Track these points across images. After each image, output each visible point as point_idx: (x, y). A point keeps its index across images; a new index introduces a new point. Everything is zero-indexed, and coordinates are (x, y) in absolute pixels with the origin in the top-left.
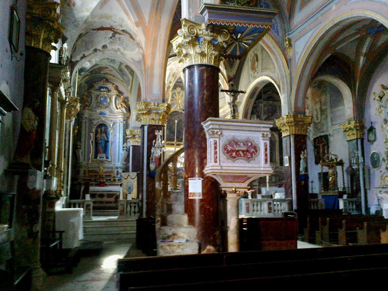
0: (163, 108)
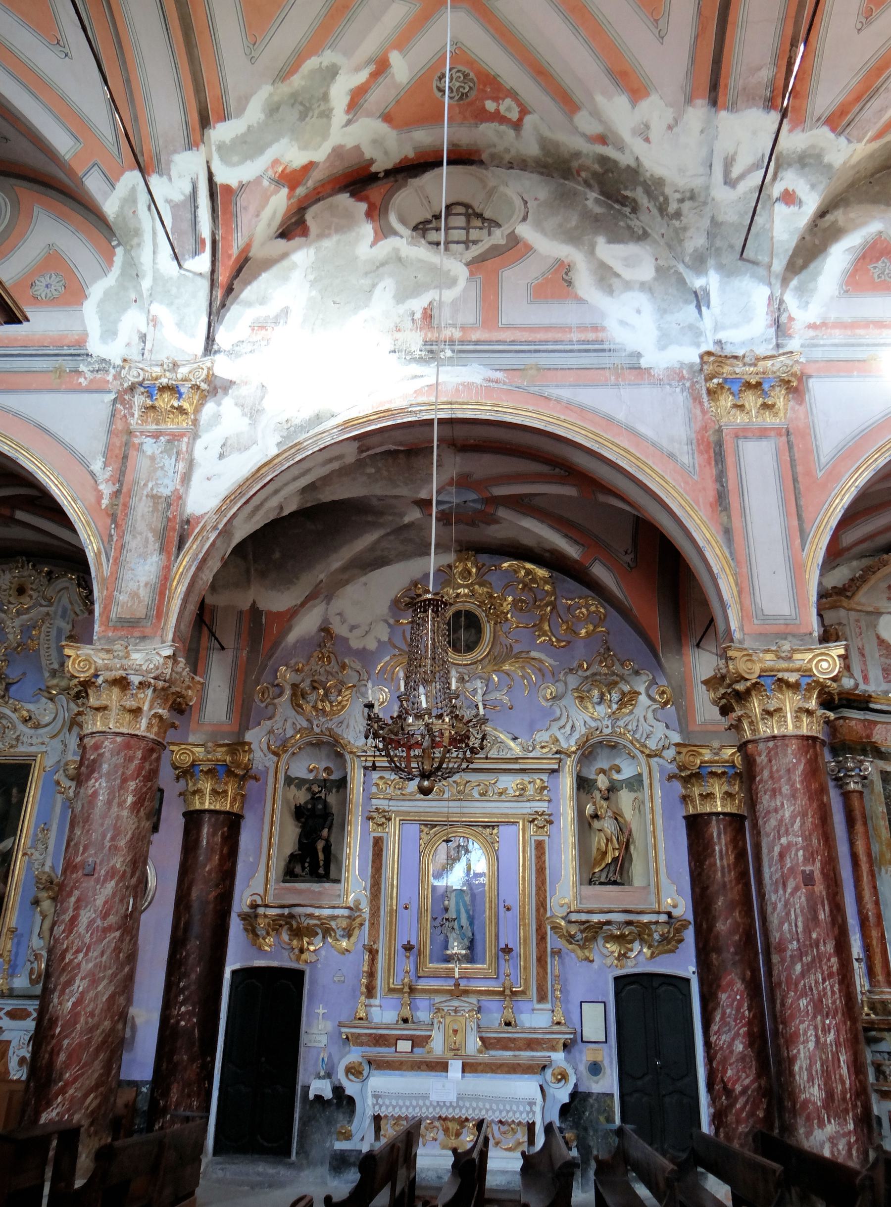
0: (825, 665)
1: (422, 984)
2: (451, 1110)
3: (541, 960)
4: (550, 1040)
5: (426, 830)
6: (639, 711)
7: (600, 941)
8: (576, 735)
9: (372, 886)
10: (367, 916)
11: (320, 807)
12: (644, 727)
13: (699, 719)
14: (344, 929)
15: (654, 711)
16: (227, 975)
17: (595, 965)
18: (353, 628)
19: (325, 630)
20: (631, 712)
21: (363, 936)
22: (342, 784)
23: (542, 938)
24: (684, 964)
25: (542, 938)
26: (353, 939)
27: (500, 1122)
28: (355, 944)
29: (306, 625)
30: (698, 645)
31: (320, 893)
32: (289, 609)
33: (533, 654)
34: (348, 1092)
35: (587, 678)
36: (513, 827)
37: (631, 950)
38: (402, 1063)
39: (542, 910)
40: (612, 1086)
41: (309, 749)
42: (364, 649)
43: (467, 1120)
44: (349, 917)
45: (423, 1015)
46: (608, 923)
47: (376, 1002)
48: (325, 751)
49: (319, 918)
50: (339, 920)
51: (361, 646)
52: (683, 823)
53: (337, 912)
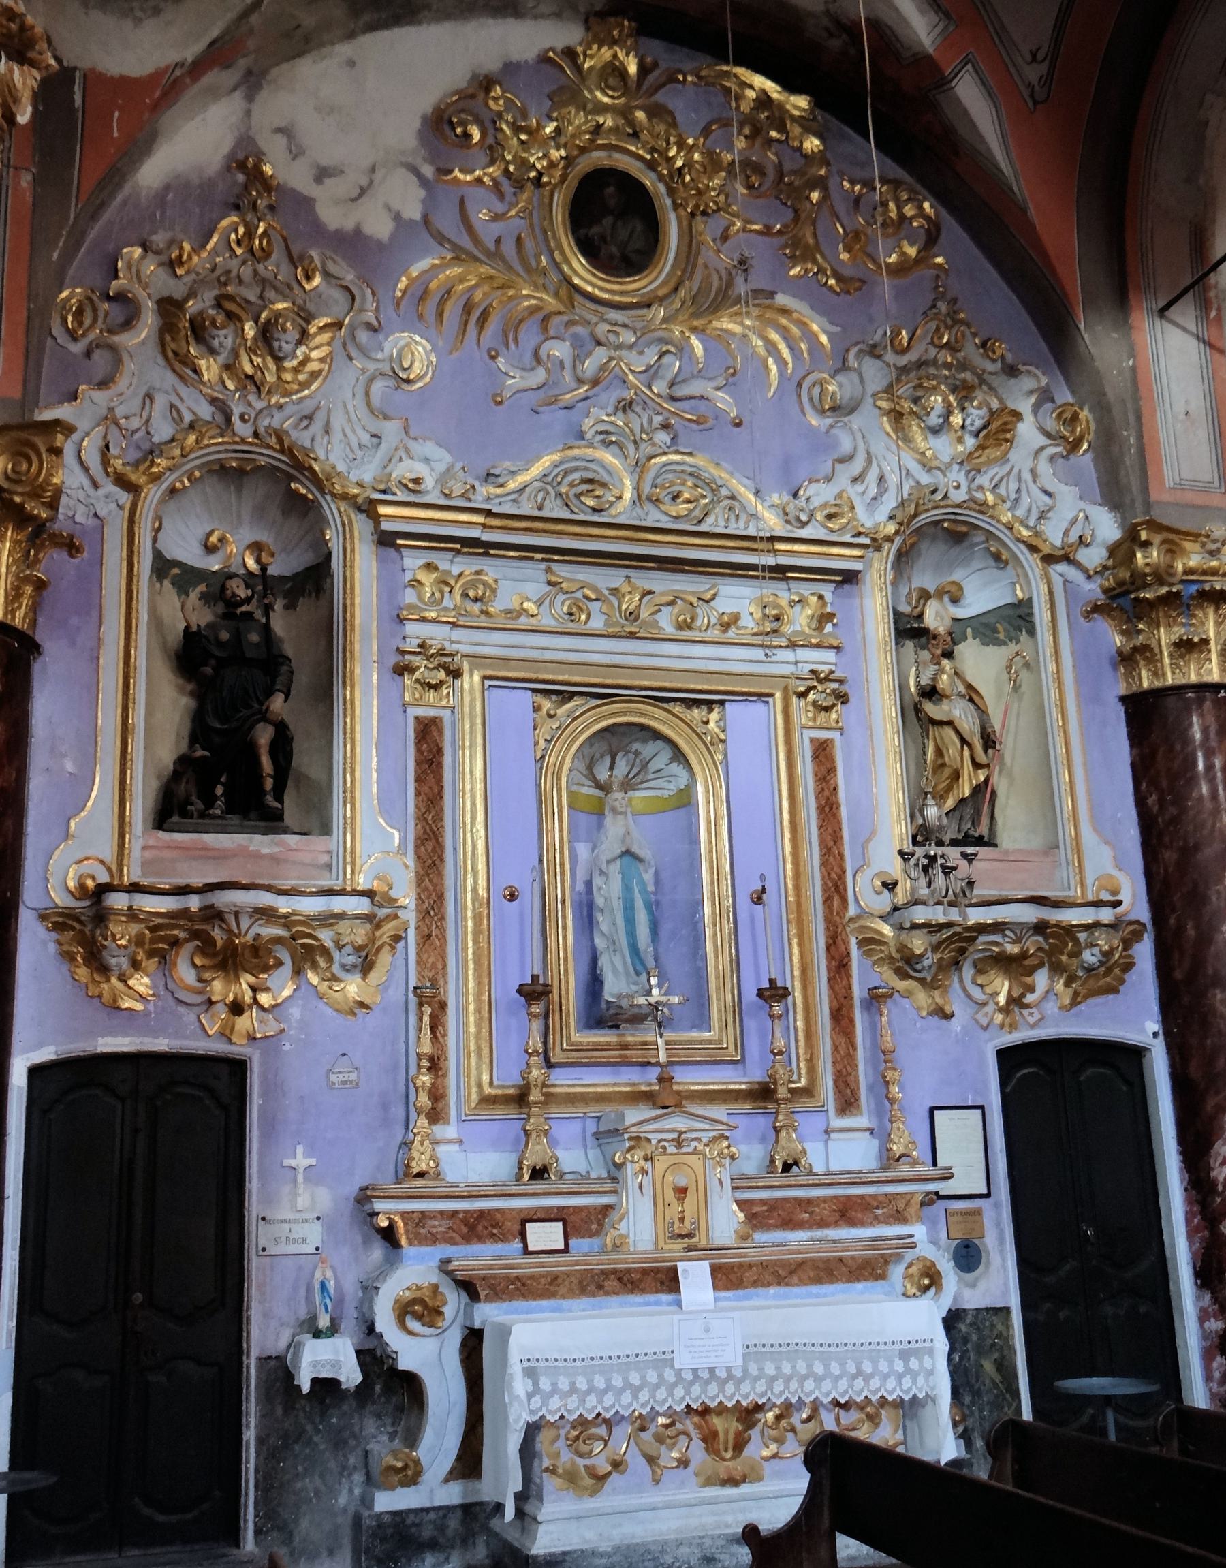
1: (563, 1080)
2: (730, 1388)
3: (841, 1017)
4: (891, 1198)
5: (547, 705)
6: (1019, 457)
7: (968, 971)
8: (890, 502)
9: (420, 842)
10: (410, 916)
11: (254, 637)
12: (1033, 499)
13: (1170, 477)
14: (358, 949)
15: (1052, 459)
16: (18, 1078)
17: (956, 1025)
18: (322, 174)
19: (246, 167)
20: (1004, 459)
21: (398, 970)
22: (315, 581)
23: (839, 966)
24: (1133, 1017)
25: (839, 966)
26: (375, 976)
27: (836, 1403)
28: (383, 988)
29: (193, 143)
30: (1162, 312)
31: (274, 859)
32: (156, 76)
33: (781, 299)
34: (404, 1364)
35: (904, 370)
36: (758, 708)
37: (1031, 989)
38: (555, 1279)
39: (836, 902)
40: (1006, 1292)
41: (213, 487)
42: (358, 232)
43: (758, 1408)
44: (368, 918)
45: (572, 1156)
46: (998, 927)
47: (449, 1131)
48: (255, 491)
49: (286, 920)
50: (343, 926)
51: (349, 225)
52: (1120, 710)
53: (339, 904)
